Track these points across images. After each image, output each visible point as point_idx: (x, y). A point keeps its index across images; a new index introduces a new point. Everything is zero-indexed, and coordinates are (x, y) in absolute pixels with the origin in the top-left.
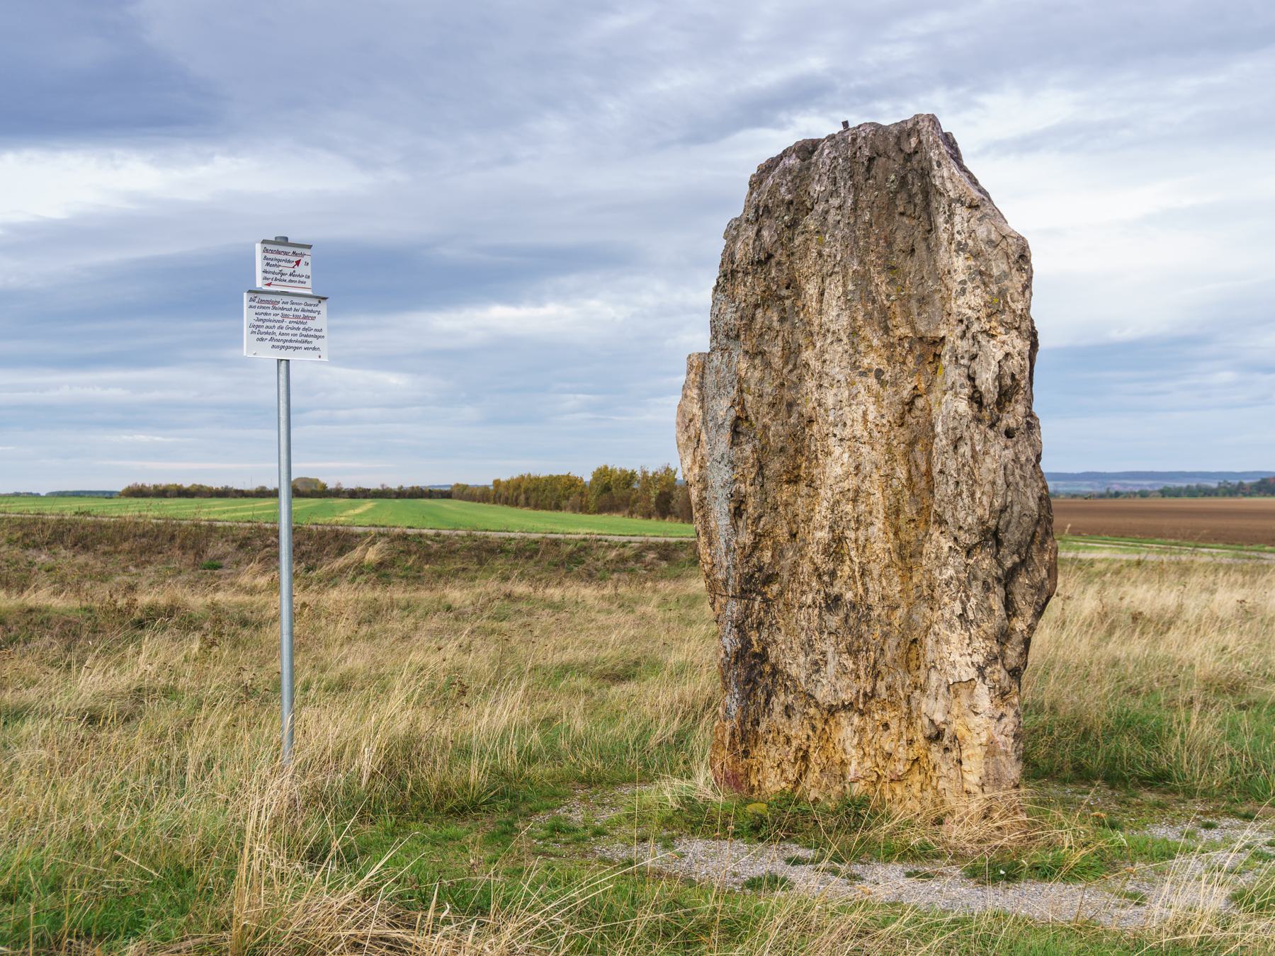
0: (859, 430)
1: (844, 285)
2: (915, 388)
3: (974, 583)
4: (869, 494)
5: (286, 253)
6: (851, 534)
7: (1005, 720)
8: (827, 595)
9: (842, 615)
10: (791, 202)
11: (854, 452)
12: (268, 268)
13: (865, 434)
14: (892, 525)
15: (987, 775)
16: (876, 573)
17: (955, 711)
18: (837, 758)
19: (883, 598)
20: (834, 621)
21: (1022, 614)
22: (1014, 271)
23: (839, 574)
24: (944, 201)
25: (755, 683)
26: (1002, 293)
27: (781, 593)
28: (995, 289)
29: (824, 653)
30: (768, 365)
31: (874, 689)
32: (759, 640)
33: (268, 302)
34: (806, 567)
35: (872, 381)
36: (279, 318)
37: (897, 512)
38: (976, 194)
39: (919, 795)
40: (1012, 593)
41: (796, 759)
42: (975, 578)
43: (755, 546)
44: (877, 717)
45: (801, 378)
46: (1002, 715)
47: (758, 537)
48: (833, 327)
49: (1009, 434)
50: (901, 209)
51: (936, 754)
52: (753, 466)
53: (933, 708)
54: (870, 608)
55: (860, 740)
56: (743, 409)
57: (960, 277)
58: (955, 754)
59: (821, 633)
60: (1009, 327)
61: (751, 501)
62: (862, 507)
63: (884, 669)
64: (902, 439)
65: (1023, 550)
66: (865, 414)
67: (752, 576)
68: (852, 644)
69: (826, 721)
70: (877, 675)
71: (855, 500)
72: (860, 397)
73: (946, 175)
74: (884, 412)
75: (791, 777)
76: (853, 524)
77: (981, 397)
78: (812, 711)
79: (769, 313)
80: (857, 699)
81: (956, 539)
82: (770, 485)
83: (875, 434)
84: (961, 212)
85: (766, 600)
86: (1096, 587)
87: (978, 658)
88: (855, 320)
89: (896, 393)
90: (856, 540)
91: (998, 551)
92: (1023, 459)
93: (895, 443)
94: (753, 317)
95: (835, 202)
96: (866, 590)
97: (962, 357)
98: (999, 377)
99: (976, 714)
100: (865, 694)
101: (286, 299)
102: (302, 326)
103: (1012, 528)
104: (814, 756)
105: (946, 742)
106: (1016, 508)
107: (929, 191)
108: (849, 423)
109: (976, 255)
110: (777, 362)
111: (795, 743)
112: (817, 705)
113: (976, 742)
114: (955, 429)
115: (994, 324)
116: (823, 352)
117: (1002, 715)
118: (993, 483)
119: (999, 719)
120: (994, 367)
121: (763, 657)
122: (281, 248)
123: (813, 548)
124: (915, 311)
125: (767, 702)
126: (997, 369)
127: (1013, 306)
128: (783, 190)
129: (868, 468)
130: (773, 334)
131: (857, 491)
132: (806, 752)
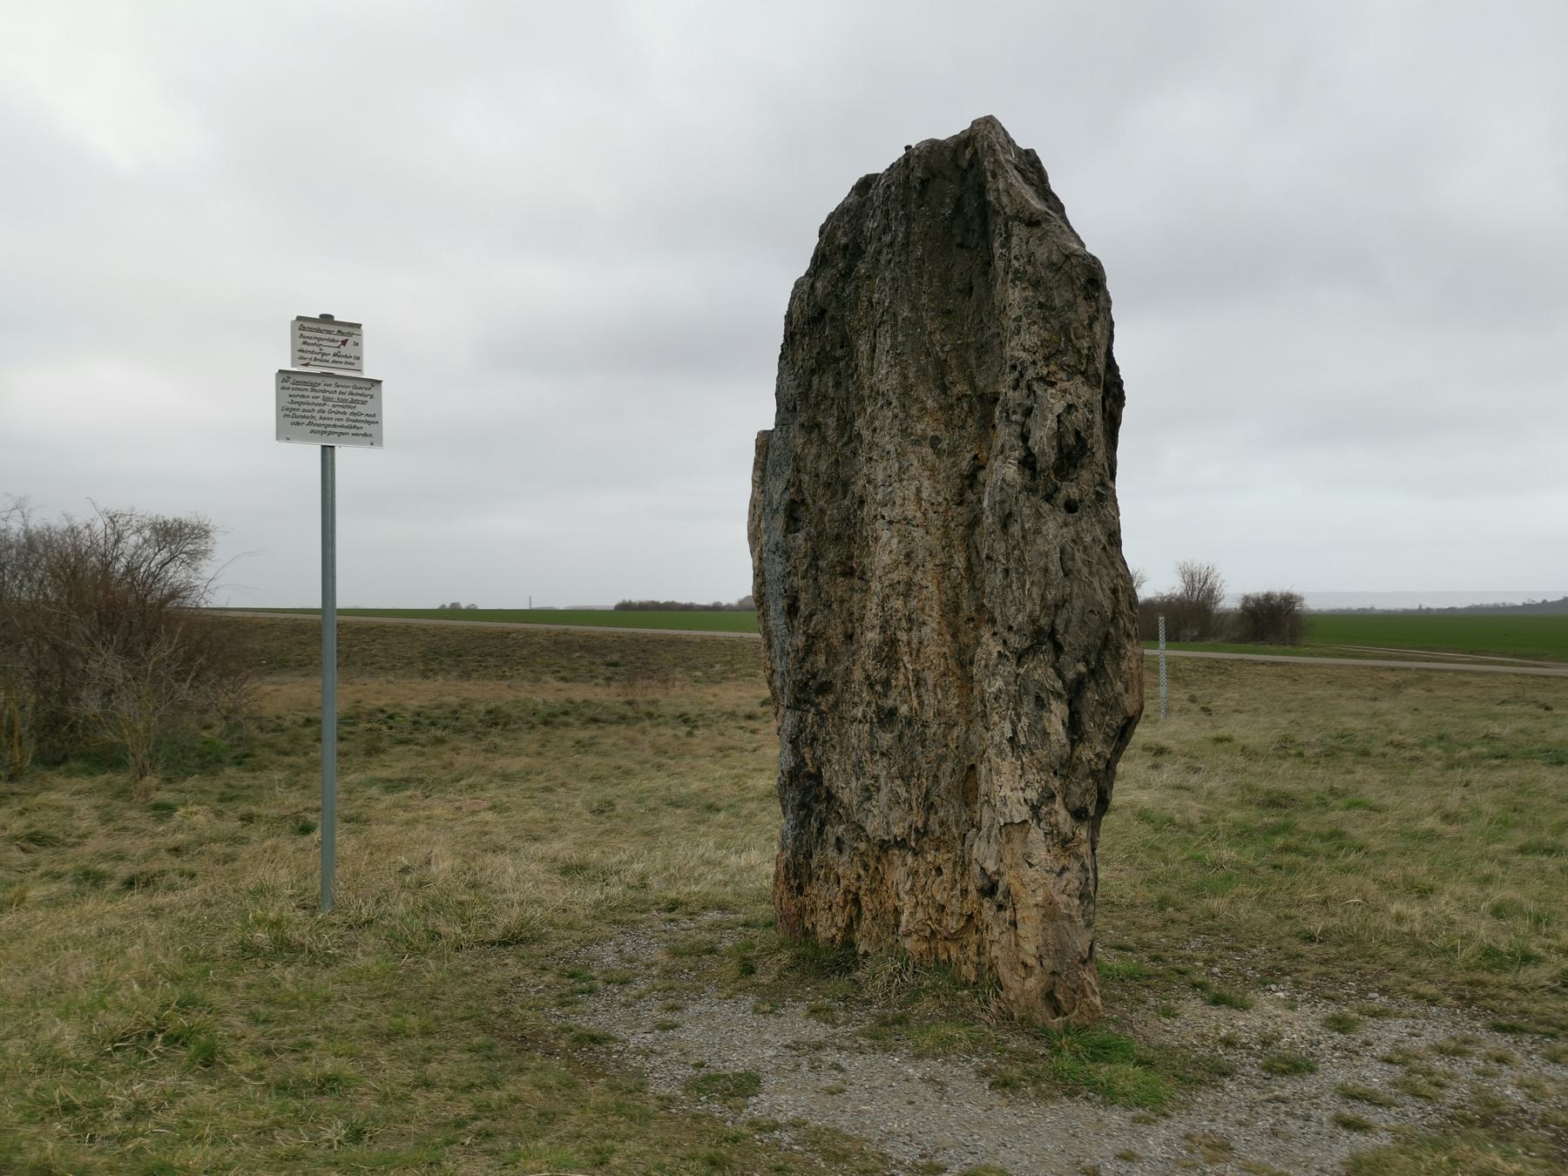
0: (911, 510)
1: (894, 337)
2: (976, 457)
3: (1025, 698)
4: (922, 587)
5: (329, 332)
6: (902, 636)
7: (1067, 875)
8: (880, 709)
9: (896, 733)
10: (846, 247)
11: (903, 538)
12: (305, 347)
13: (919, 515)
14: (950, 625)
15: (1046, 944)
16: (930, 682)
17: (1008, 861)
18: (889, 905)
19: (939, 714)
20: (886, 739)
21: (1089, 740)
22: (1079, 300)
23: (894, 683)
24: (1000, 220)
25: (810, 810)
26: (1065, 329)
27: (836, 705)
28: (1056, 324)
29: (876, 778)
30: (824, 440)
31: (925, 824)
32: (813, 758)
33: (305, 383)
34: (858, 675)
35: (927, 450)
36: (320, 401)
37: (957, 608)
38: (1037, 204)
39: (975, 959)
40: (1078, 712)
41: (846, 902)
42: (1027, 693)
43: (809, 650)
44: (930, 858)
45: (855, 453)
46: (1064, 869)
47: (812, 639)
48: (883, 388)
49: (1071, 507)
50: (958, 240)
51: (988, 911)
52: (805, 556)
53: (984, 854)
54: (925, 725)
55: (913, 885)
56: (800, 490)
57: (1014, 312)
58: (1008, 914)
59: (873, 753)
60: (1072, 372)
61: (803, 595)
62: (914, 603)
63: (937, 801)
64: (960, 520)
65: (1093, 658)
66: (919, 490)
67: (806, 684)
68: (903, 767)
69: (878, 859)
70: (930, 808)
71: (906, 595)
72: (913, 471)
73: (1001, 186)
74: (939, 487)
75: (840, 924)
76: (904, 624)
77: (1035, 462)
78: (863, 846)
79: (824, 379)
80: (909, 835)
81: (1005, 642)
82: (823, 579)
83: (931, 514)
84: (1019, 231)
85: (819, 713)
86: (57, 1047)
87: (1032, 795)
88: (905, 377)
89: (954, 465)
90: (909, 643)
91: (1058, 658)
92: (1088, 539)
93: (952, 525)
94: (810, 386)
95: (887, 239)
96: (921, 703)
97: (1015, 412)
98: (1059, 435)
99: (1031, 865)
100: (917, 830)
101: (328, 380)
102: (349, 411)
103: (1074, 628)
104: (865, 900)
105: (999, 897)
106: (1078, 603)
107: (985, 212)
108: (899, 501)
109: (1036, 285)
110: (831, 434)
111: (843, 883)
112: (868, 840)
113: (1032, 902)
114: (1002, 502)
115: (1053, 368)
116: (873, 419)
117: (1064, 869)
118: (1046, 570)
119: (1060, 874)
120: (1051, 423)
121: (817, 777)
122: (323, 327)
123: (864, 652)
124: (973, 362)
125: (820, 831)
126: (1055, 425)
127: (1078, 344)
128: (840, 233)
129: (921, 554)
130: (828, 403)
131: (909, 584)
132: (857, 894)
